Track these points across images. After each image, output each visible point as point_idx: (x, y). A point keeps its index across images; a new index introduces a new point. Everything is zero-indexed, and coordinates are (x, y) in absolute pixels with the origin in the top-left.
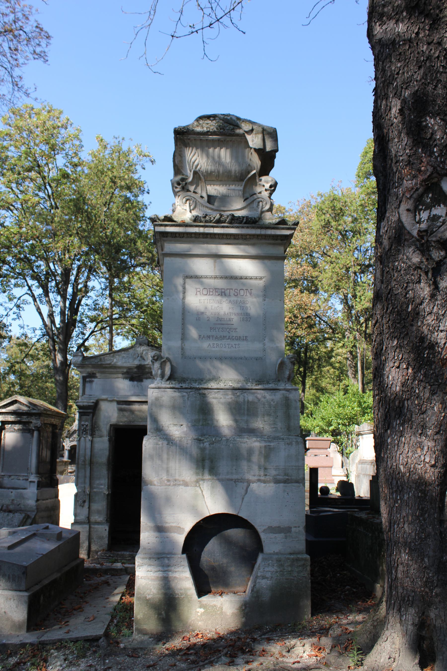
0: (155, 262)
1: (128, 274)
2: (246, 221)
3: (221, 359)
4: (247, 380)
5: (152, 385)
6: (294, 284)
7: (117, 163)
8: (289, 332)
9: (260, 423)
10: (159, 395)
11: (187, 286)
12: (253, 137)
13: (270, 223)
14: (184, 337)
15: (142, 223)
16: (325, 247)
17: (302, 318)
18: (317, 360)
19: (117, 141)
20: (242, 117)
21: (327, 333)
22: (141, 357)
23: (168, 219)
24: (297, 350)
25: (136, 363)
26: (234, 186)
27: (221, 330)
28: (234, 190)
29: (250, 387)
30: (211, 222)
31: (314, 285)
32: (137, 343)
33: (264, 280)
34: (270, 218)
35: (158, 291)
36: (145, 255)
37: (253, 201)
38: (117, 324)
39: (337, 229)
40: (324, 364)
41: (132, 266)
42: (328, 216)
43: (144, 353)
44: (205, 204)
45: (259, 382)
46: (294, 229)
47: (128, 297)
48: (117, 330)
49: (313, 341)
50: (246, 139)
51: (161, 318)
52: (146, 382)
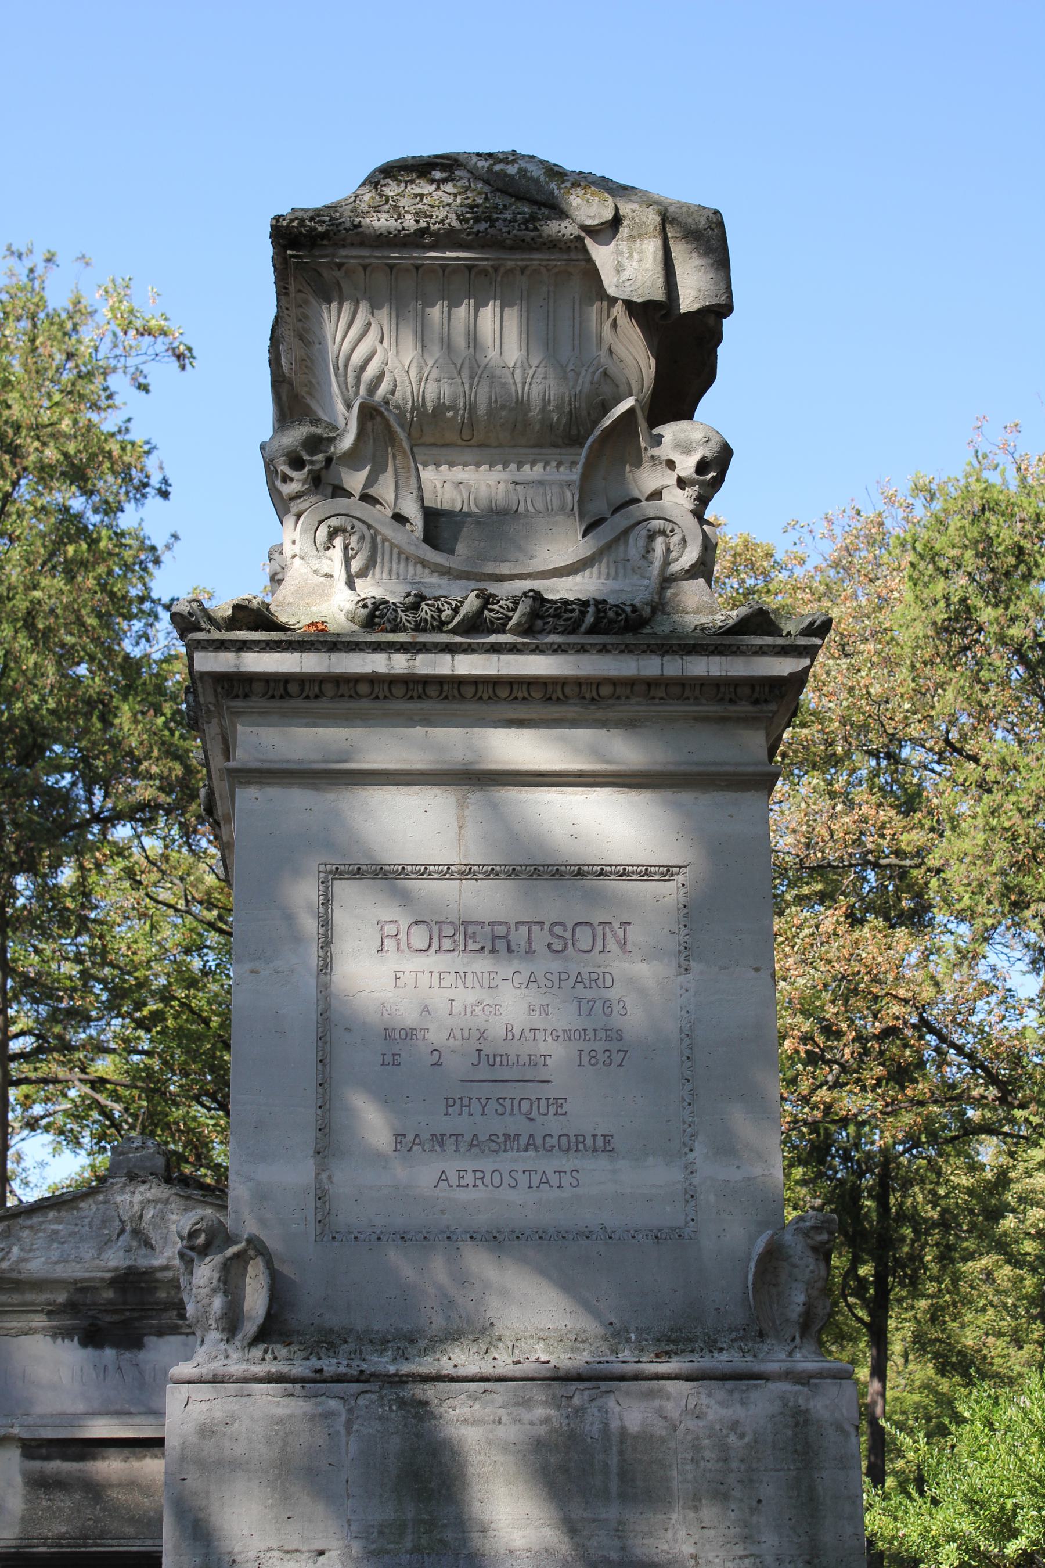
0: (197, 802)
1: (79, 853)
2: (598, 620)
3: (499, 1240)
4: (617, 1335)
5: (184, 1369)
6: (819, 887)
7: (25, 365)
8: (806, 1100)
9: (682, 1533)
10: (218, 1414)
11: (340, 917)
12: (619, 253)
13: (704, 628)
14: (328, 1141)
15: (137, 625)
16: (953, 721)
17: (859, 1038)
18: (935, 1225)
19: (21, 270)
20: (570, 165)
21: (979, 1102)
22: (136, 1233)
23: (252, 617)
24: (842, 1182)
25: (112, 1264)
26: (539, 468)
27: (492, 1105)
28: (541, 483)
29: (630, 1368)
30: (441, 626)
31: (909, 888)
32: (113, 1170)
33: (680, 878)
34: (702, 607)
35: (212, 925)
36: (154, 770)
37: (626, 532)
38: (27, 1081)
39: (1002, 639)
40: (970, 1244)
41: (96, 818)
42: (964, 581)
43: (149, 1214)
44: (411, 550)
45: (671, 1342)
46: (811, 652)
47: (78, 959)
48: (26, 1107)
49: (913, 1141)
50: (590, 261)
51: (227, 1046)
52: (159, 1350)
